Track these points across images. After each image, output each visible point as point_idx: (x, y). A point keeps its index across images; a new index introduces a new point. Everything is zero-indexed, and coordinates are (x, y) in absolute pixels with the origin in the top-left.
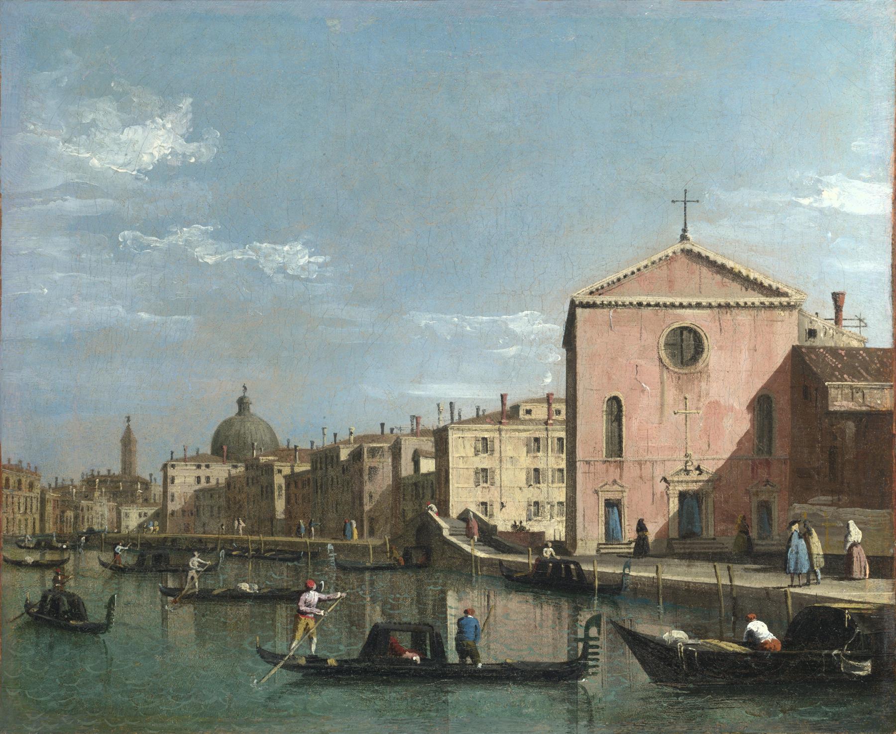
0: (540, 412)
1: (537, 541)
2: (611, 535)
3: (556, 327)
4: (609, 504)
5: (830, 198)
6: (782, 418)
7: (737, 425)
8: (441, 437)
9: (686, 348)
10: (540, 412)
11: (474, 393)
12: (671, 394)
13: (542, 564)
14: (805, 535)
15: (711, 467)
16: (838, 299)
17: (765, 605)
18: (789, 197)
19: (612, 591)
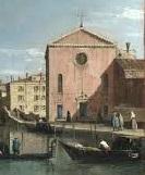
0: (38, 79)
1: (37, 117)
2: (59, 116)
3: (137, 35)
4: (59, 106)
5: (125, 15)
6: (111, 77)
7: (98, 82)
8: (8, 86)
9: (82, 59)
10: (38, 79)
11: (18, 72)
12: (77, 73)
13: (38, 124)
14: (118, 116)
15: (90, 94)
16: (128, 45)
17: (106, 137)
18: (111, 14)
19: (60, 133)
